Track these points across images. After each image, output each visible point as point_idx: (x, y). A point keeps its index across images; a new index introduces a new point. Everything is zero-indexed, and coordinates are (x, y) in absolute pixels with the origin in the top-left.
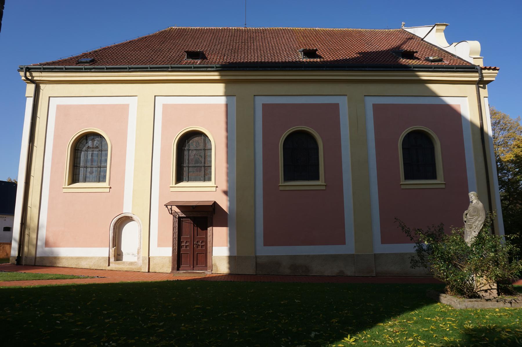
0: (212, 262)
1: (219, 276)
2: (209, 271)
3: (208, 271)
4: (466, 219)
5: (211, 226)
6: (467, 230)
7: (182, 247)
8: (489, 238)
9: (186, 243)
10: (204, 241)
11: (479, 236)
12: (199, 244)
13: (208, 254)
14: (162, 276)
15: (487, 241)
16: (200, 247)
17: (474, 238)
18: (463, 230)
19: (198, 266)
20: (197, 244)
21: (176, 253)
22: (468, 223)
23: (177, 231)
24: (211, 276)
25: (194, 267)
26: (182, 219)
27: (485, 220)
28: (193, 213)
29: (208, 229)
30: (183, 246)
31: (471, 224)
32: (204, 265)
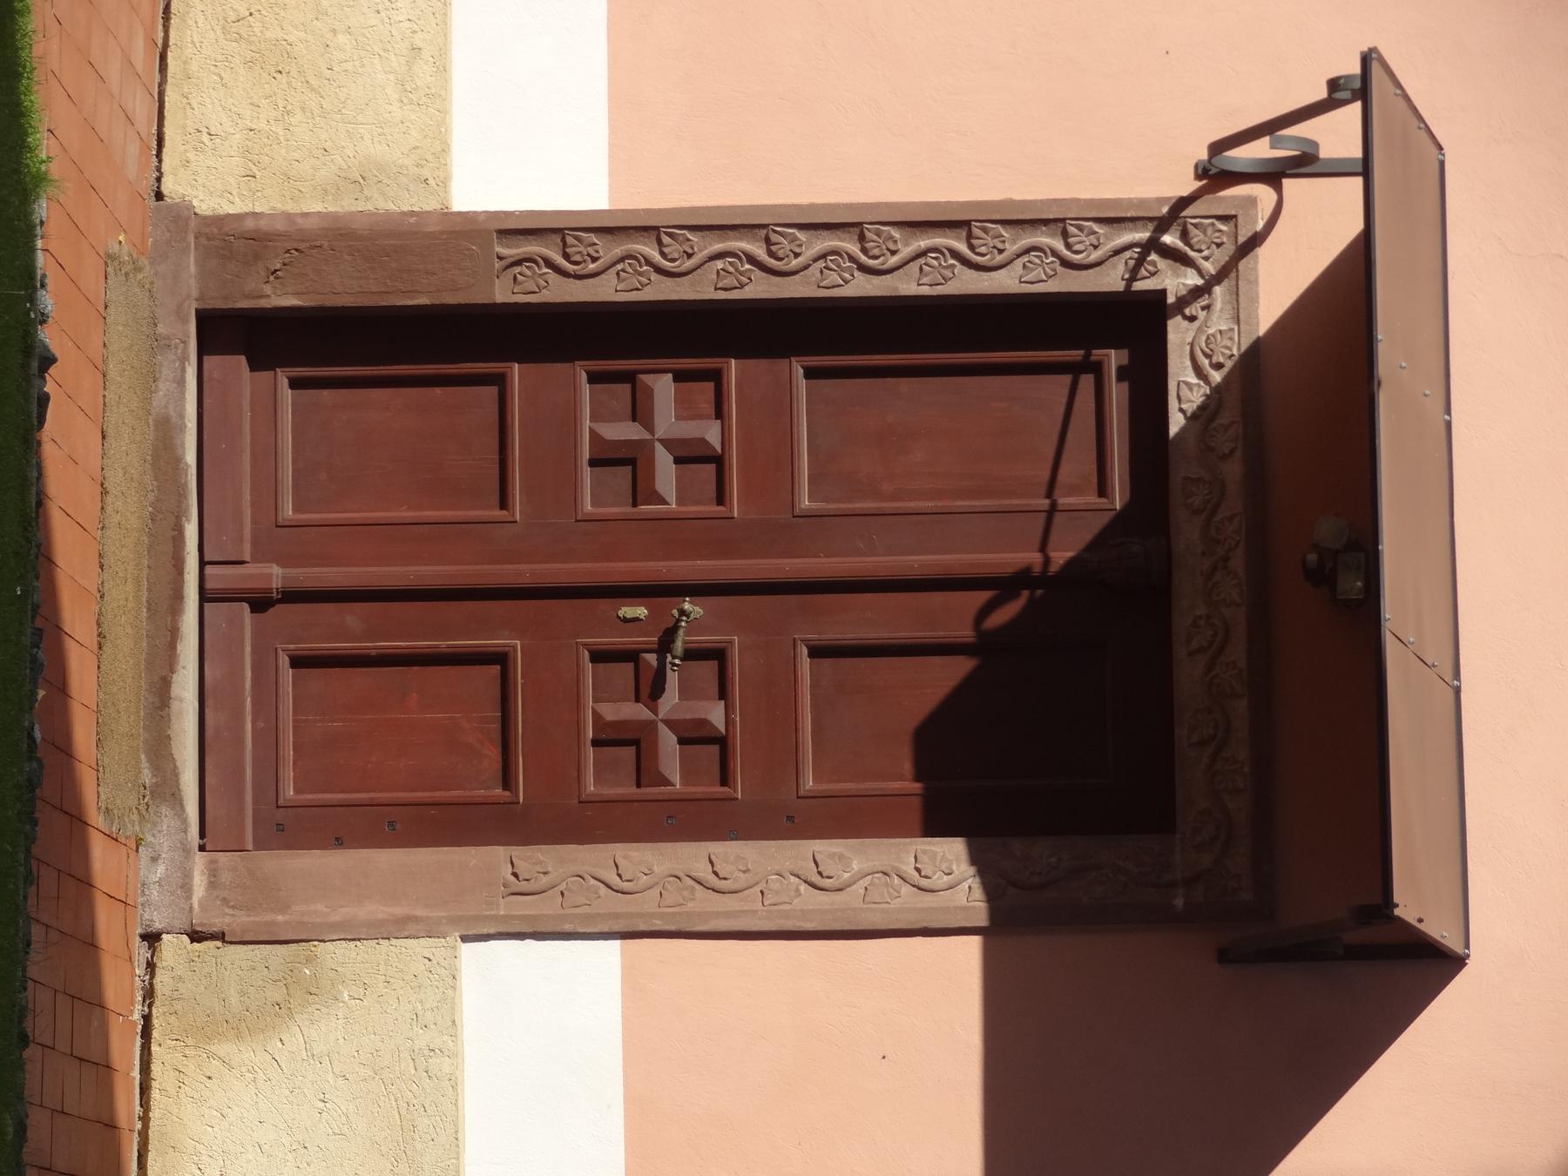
0: (353, 933)
1: (104, 1068)
2: (187, 888)
3: (200, 860)
5: (993, 894)
7: (624, 389)
9: (689, 455)
10: (725, 779)
12: (672, 679)
13: (500, 853)
14: (113, 71)
16: (611, 712)
19: (287, 674)
20: (665, 644)
21: (502, 293)
23: (907, 285)
24: (108, 924)
25: (260, 603)
26: (1114, 359)
28: (1238, 563)
29: (950, 855)
30: (640, 411)
32: (289, 792)
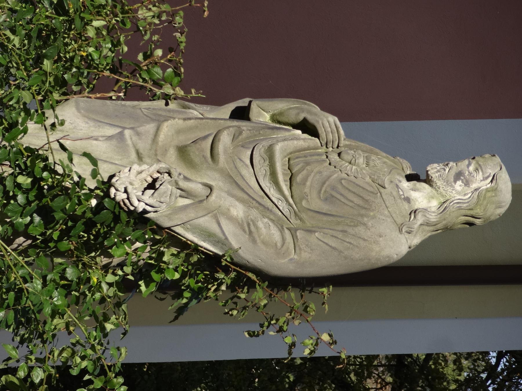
4: (266, 118)
6: (167, 128)
8: (99, 287)
11: (117, 219)
15: (70, 273)
17: (95, 174)
18: (168, 89)
22: (225, 139)
27: (258, 272)
31: (222, 158)
